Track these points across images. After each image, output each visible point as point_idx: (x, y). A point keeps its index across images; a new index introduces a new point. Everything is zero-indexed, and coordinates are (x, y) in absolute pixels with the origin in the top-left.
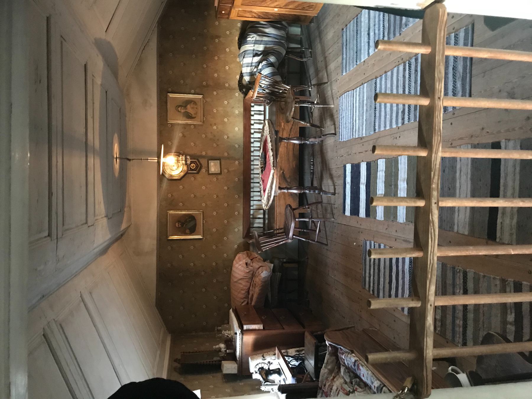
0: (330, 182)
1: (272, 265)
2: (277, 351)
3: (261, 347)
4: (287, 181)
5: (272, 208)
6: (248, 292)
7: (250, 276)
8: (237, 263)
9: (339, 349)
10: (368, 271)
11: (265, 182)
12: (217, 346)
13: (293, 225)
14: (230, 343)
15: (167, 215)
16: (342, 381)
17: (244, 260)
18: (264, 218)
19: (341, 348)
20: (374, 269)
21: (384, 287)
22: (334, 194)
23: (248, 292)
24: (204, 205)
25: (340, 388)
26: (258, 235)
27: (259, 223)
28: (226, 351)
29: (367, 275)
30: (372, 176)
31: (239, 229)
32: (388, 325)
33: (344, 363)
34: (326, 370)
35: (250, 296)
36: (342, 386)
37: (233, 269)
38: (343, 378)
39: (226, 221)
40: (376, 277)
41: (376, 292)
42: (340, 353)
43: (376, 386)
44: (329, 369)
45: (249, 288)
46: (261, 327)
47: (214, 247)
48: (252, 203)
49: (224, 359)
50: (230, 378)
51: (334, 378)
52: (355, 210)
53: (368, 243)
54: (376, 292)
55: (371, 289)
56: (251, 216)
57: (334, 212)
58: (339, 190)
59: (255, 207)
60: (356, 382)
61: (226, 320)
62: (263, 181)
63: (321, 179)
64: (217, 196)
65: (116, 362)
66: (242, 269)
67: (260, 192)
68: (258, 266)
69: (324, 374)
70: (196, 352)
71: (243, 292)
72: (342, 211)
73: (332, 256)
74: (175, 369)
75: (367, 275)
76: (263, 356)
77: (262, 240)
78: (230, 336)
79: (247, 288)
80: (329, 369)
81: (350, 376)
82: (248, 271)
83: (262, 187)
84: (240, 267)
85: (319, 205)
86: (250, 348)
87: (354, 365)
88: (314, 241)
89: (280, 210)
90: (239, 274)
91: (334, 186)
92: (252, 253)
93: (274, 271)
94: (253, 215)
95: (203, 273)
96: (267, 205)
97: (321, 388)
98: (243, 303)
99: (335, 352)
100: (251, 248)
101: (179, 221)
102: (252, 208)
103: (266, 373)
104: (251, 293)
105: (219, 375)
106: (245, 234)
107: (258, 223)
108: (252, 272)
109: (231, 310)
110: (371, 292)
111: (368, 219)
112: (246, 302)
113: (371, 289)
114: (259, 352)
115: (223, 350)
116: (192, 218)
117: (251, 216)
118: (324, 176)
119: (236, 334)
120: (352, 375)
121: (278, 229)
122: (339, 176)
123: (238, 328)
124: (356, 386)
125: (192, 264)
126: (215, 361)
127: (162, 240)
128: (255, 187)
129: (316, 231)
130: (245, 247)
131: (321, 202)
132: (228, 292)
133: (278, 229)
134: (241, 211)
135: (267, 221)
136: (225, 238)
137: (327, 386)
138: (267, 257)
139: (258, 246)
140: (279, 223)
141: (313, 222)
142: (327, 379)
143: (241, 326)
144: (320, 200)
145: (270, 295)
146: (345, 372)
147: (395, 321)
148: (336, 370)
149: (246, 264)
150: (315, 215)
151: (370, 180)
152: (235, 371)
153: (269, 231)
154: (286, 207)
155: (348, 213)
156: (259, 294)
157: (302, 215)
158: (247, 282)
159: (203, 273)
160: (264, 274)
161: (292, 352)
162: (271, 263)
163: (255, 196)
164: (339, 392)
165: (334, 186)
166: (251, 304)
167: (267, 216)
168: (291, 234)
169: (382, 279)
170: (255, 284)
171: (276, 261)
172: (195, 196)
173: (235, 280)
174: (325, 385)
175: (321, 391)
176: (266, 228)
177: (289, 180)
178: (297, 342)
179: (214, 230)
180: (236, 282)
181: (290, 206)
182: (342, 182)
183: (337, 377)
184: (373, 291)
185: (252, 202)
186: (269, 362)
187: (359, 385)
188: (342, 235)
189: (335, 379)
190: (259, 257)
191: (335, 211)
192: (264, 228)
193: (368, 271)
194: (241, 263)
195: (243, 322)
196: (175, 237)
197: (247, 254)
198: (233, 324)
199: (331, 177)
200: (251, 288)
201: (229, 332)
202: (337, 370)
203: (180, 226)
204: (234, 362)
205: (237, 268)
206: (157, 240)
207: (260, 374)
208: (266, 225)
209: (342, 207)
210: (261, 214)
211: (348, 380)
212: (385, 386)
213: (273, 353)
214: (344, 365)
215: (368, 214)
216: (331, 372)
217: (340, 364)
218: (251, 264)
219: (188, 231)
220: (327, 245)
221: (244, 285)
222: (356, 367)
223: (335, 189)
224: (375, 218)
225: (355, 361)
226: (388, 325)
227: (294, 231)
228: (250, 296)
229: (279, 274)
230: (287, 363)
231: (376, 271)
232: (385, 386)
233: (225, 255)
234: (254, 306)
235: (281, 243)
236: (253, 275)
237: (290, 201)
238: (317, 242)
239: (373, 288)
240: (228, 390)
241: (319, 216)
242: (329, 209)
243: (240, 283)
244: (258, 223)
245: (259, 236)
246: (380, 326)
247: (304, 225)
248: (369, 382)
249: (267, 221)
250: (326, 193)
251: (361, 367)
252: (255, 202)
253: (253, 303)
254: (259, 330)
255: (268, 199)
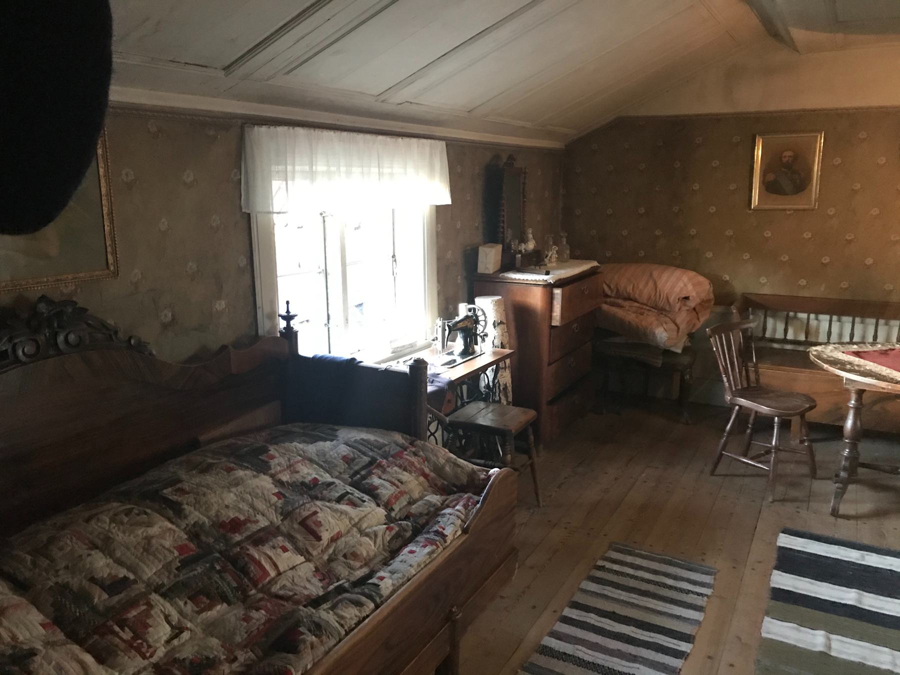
0: (866, 507)
1: (679, 351)
2: (507, 351)
3: (519, 319)
4: (875, 403)
5: (811, 365)
6: (629, 298)
7: (661, 304)
8: (690, 279)
9: (476, 498)
10: (644, 563)
11: (883, 359)
12: (531, 236)
13: (764, 409)
14: (534, 262)
15: (811, 131)
16: (416, 495)
17: (694, 294)
18: (785, 341)
19: (478, 502)
20: (649, 581)
21: (606, 597)
22: (835, 513)
23: (629, 298)
24: (831, 211)
25: (402, 488)
26: (747, 329)
27: (774, 330)
28: (520, 252)
29: (638, 561)
30: (880, 630)
31: (765, 285)
32: (528, 587)
33: (448, 506)
34: (442, 461)
35: (620, 301)
36: (405, 493)
37: (678, 272)
38: (421, 498)
39: (785, 258)
40: (632, 583)
41: (599, 574)
42: (469, 499)
43: (382, 584)
44: (443, 467)
45: (636, 301)
46: (557, 320)
47: (729, 233)
48: (824, 318)
49: (506, 251)
50: (471, 258)
51: (426, 476)
52: (790, 562)
53: (707, 579)
54: (599, 574)
55: (608, 565)
56: (791, 314)
57: (788, 504)
58: (845, 529)
59: (813, 323)
60: (405, 530)
61: (576, 256)
62: (885, 353)
63: (875, 486)
64: (850, 242)
65: (503, 33)
66: (677, 289)
67: (851, 342)
68: (678, 321)
69: (436, 455)
70: (524, 197)
71: (630, 289)
72: (790, 525)
73: (687, 482)
74: (497, 157)
75: (638, 561)
76: (501, 323)
77: (736, 338)
78: (546, 260)
79: (637, 296)
80: (443, 467)
81: (421, 514)
82: (671, 300)
83: (869, 348)
84: (681, 284)
85: (805, 470)
86: (519, 298)
87: (437, 533)
88: (724, 449)
89: (801, 381)
90: (667, 281)
91: (856, 517)
92: (709, 311)
93: (667, 353)
94: (795, 317)
95: (676, 209)
96: (819, 357)
97: (412, 444)
98: (609, 287)
99: (474, 486)
100: (720, 309)
101: (795, 158)
102: (812, 316)
103: (469, 332)
104: (626, 304)
105: (479, 237)
106: (754, 298)
107: (775, 328)
108: (667, 308)
109: (595, 264)
110: (600, 563)
111: (766, 595)
112: (609, 293)
113: (608, 565)
114: (511, 316)
115: (523, 247)
116: (801, 185)
117: (791, 314)
118: (882, 495)
119: (547, 273)
120: (422, 521)
121: (757, 372)
122: (882, 536)
123: (557, 278)
124: (397, 529)
125: (696, 187)
126: (503, 233)
127: (752, 125)
128: (865, 328)
129: (745, 456)
130: (723, 297)
131: (813, 475)
132: (632, 258)
133: (757, 372)
134: (806, 294)
135: (776, 346)
136: (746, 256)
137: (413, 459)
138: (696, 342)
139: (723, 327)
140: (771, 374)
141: (768, 452)
142: (427, 459)
143: (560, 284)
144: (819, 473)
145: (618, 340)
146: (429, 504)
147: (534, 607)
148: (440, 482)
149: (687, 298)
150: (782, 455)
151: (869, 621)
152: (481, 269)
153: (755, 349)
154: (809, 398)
155: (785, 541)
156: (622, 322)
157: (785, 425)
158: (650, 298)
159: (676, 209)
160: (662, 334)
161: (506, 377)
162: (685, 350)
163: (844, 326)
164: (394, 484)
165: (856, 517)
166: (606, 303)
167: (789, 347)
168: (743, 401)
169: (623, 595)
170: (642, 314)
171: (686, 360)
172: (855, 192)
173: (655, 274)
174: (415, 454)
175: (407, 444)
176: (762, 344)
177: (877, 408)
178: (523, 392)
179: (768, 234)
180: (651, 275)
181: (811, 408)
182: (866, 541)
183: (426, 484)
184: (601, 568)
185: (827, 317)
186: (486, 335)
187: (397, 536)
188: (732, 514)
189: (422, 479)
190: (699, 325)
191: (789, 508)
192: (763, 338)
193: (644, 563)
194: (690, 287)
195: (567, 288)
196: (759, 153)
197: (708, 301)
198: (569, 267)
199: (879, 514)
200: (636, 304)
201: (554, 260)
202: (439, 484)
203: (785, 160)
204: (498, 266)
205: (679, 279)
206: (757, 113)
207: (467, 317)
208: (769, 345)
209: (799, 528)
210: (795, 333)
211: (414, 509)
212: (377, 607)
213: (505, 342)
214: (444, 506)
215: (781, 595)
216: (438, 470)
217: (450, 493)
218: (684, 308)
219: (771, 177)
220: (712, 473)
221: (644, 290)
222: (431, 536)
223: (847, 517)
224: (767, 613)
225: (444, 536)
226: (528, 587)
227: (750, 410)
228: (620, 301)
229: (659, 362)
230: (484, 369)
231: (644, 587)
232: (377, 607)
233: (709, 255)
234: (600, 308)
235: (725, 379)
236: (662, 310)
237: (824, 405)
238: (722, 455)
239: (610, 571)
240: (449, 255)
241: (780, 466)
242: (793, 493)
243: (647, 283)
244: (775, 328)
245: (745, 331)
246: (532, 568)
247: (763, 425)
248: (396, 564)
249: (776, 346)
250: (840, 495)
251: (428, 549)
252: (825, 326)
253: (605, 307)
254: (551, 317)
255: (835, 363)
